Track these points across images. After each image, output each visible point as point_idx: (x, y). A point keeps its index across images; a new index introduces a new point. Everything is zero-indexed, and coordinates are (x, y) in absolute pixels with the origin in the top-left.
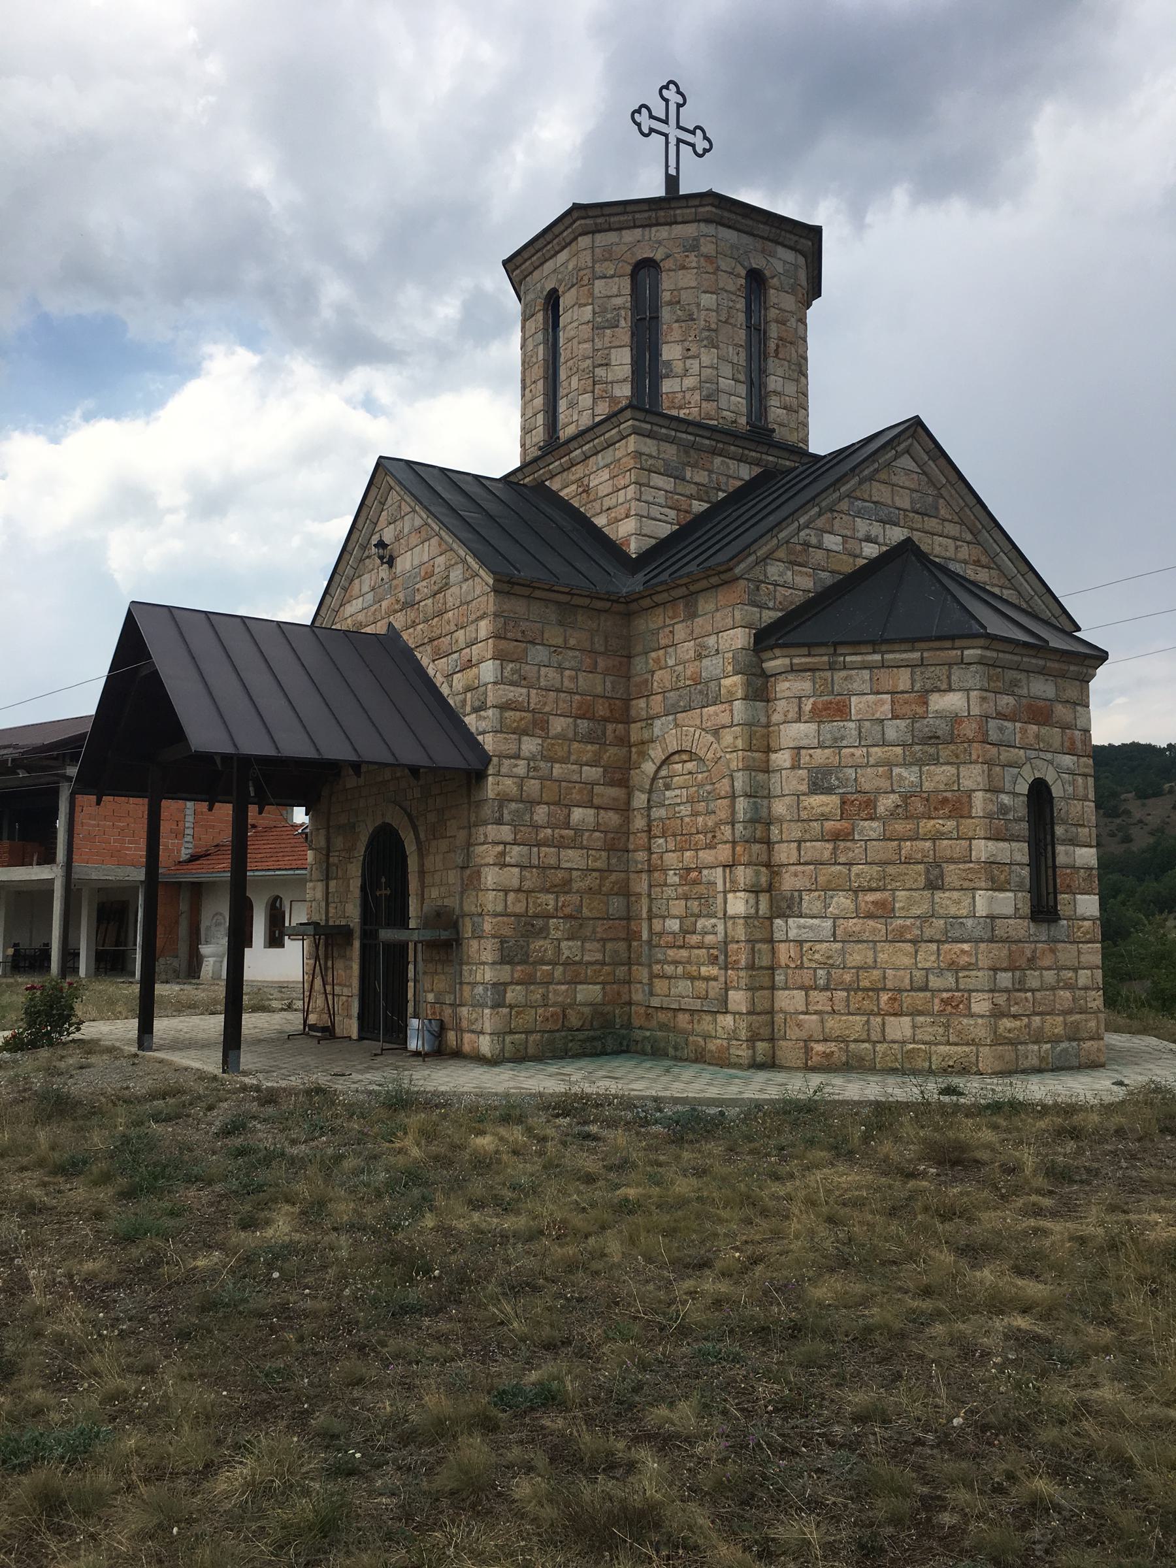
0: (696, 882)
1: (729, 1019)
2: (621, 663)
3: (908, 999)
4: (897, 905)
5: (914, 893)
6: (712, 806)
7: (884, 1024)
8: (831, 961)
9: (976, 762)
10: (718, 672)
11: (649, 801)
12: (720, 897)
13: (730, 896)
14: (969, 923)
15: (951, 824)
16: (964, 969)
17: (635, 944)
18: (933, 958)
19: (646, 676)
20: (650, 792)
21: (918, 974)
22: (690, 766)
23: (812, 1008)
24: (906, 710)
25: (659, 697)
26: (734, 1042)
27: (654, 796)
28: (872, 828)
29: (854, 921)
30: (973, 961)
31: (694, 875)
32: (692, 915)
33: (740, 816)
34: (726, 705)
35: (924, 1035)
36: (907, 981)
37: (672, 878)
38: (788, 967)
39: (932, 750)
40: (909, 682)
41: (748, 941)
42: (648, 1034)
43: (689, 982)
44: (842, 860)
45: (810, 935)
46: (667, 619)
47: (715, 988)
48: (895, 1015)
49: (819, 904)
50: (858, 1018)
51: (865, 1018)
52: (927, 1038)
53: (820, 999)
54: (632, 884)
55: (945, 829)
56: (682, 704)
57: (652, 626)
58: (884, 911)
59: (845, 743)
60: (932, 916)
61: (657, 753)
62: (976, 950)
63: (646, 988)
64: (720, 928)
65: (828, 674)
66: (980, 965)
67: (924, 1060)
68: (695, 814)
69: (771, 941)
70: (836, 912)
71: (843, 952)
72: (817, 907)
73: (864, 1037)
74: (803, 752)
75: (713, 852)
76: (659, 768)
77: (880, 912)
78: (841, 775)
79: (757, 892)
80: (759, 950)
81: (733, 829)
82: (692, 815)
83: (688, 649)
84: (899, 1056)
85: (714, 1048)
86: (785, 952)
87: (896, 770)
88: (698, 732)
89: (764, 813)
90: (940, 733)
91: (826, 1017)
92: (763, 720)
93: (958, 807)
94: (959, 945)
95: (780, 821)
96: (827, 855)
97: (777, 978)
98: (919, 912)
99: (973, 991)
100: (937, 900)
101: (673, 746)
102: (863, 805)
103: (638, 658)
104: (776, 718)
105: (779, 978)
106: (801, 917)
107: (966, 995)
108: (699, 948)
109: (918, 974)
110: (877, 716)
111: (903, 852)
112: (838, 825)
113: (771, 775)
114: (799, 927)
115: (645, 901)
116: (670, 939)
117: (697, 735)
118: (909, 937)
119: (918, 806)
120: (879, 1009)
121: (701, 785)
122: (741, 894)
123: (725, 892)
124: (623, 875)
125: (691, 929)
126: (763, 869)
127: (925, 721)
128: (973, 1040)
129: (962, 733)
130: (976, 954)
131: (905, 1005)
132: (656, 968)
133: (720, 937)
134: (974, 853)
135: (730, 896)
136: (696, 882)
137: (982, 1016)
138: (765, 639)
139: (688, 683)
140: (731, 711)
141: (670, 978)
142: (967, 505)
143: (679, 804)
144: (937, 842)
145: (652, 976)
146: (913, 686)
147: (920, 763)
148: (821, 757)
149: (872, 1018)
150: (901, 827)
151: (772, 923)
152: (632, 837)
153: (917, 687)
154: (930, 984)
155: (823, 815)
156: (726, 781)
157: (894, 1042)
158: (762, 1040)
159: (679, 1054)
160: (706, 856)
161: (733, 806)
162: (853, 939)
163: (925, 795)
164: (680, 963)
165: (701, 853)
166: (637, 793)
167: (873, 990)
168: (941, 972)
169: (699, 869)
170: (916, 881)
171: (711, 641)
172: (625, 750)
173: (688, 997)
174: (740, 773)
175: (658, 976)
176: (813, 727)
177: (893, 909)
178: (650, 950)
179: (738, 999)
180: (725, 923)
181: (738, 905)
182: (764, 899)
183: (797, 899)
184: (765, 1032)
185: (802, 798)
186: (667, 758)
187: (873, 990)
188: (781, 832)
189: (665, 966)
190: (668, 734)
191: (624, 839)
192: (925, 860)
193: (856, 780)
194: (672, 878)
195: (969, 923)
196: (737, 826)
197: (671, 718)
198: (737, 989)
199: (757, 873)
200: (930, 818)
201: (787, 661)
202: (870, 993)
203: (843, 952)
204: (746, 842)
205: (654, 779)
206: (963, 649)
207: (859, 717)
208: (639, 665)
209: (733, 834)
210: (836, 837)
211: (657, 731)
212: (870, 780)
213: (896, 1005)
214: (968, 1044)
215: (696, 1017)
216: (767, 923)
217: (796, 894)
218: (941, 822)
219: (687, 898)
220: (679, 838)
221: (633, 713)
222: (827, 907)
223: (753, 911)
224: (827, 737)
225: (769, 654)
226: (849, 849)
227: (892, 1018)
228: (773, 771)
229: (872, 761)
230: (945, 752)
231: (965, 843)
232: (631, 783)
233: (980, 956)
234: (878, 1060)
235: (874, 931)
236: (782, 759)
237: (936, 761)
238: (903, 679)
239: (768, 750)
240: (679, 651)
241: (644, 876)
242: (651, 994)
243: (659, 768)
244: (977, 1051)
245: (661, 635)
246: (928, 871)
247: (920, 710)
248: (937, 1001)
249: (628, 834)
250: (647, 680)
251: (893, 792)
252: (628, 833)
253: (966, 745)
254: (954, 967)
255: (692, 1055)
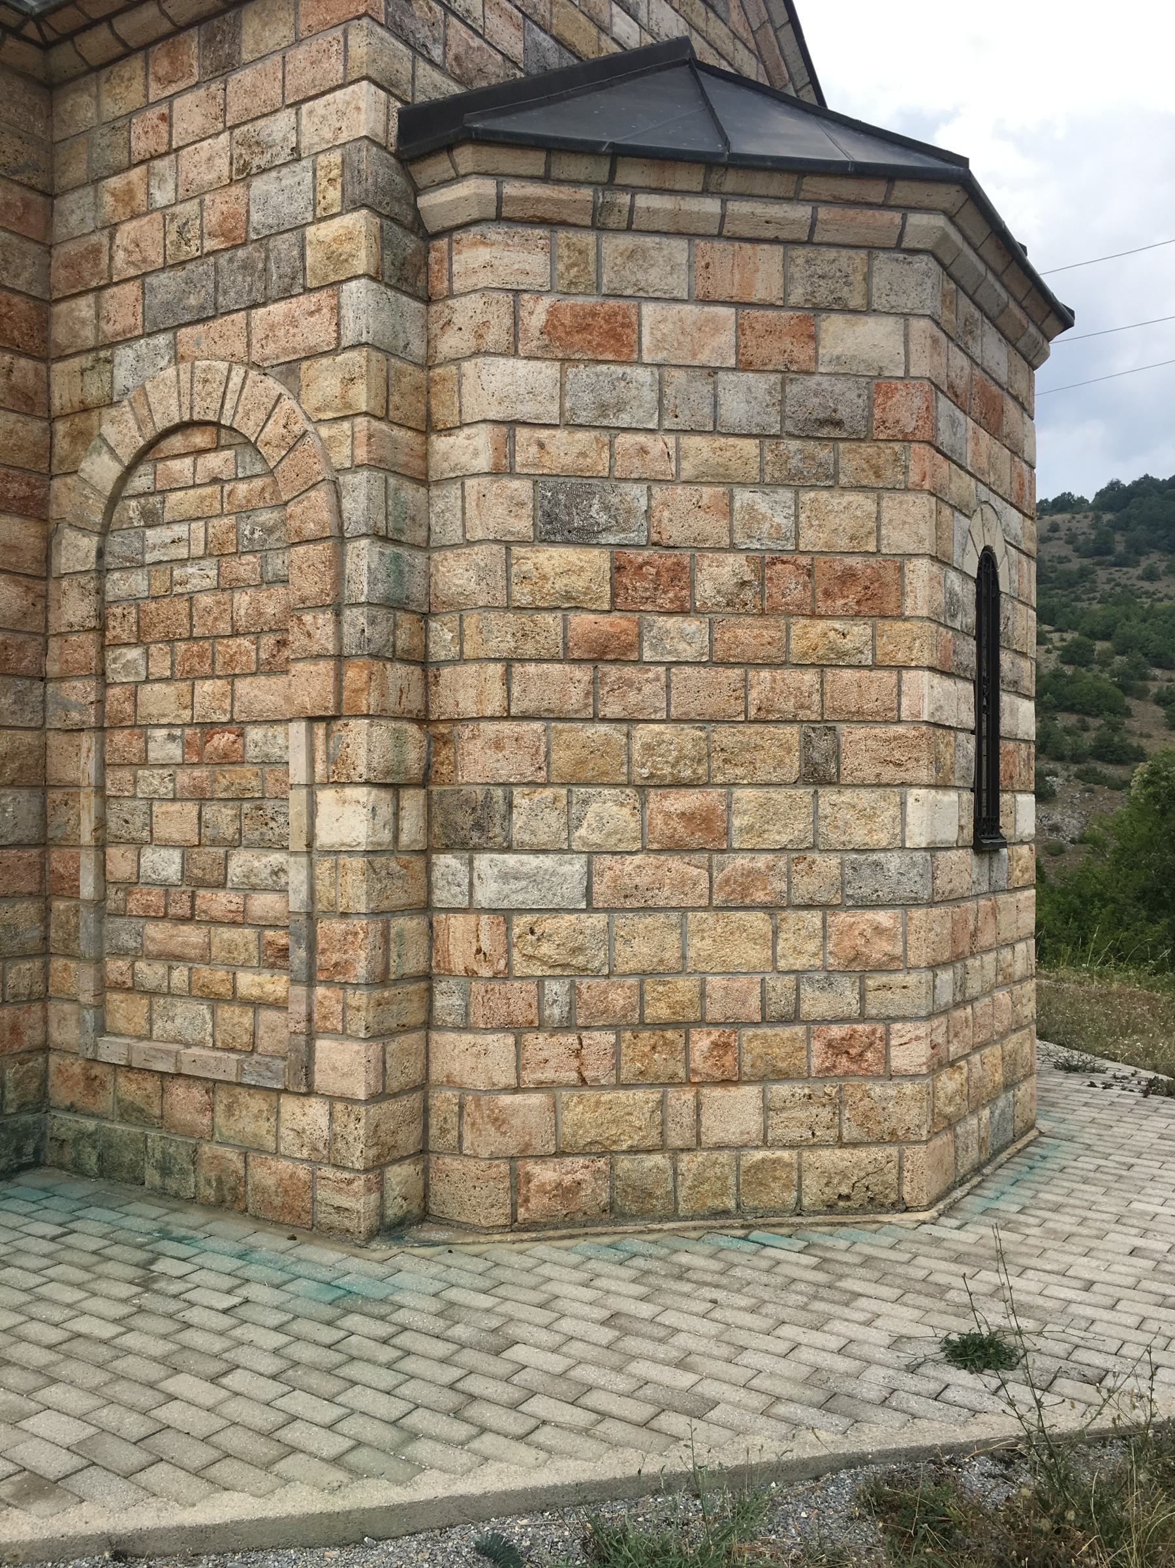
0: (227, 759)
1: (317, 1110)
2: (27, 205)
3: (755, 1044)
4: (737, 822)
5: (774, 794)
6: (277, 563)
7: (698, 1107)
8: (580, 960)
9: (918, 489)
10: (298, 208)
11: (100, 554)
12: (298, 799)
13: (326, 797)
14: (893, 862)
15: (859, 632)
16: (879, 969)
17: (60, 905)
18: (812, 946)
19: (94, 239)
20: (105, 531)
21: (781, 985)
22: (215, 462)
23: (529, 1077)
24: (770, 350)
25: (131, 291)
26: (327, 1172)
27: (116, 543)
28: (684, 635)
29: (638, 859)
30: (898, 951)
31: (222, 740)
32: (214, 842)
33: (360, 588)
34: (323, 295)
35: (788, 1128)
36: (754, 1002)
37: (163, 748)
38: (471, 974)
39: (824, 454)
40: (777, 281)
41: (374, 914)
42: (90, 1125)
43: (204, 1010)
44: (613, 709)
45: (531, 897)
46: (153, 86)
47: (275, 1030)
48: (725, 1082)
49: (553, 819)
50: (640, 1094)
51: (655, 1095)
52: (795, 1134)
53: (550, 1052)
54: (54, 759)
55: (847, 644)
56: (192, 301)
57: (112, 108)
58: (707, 836)
59: (625, 420)
60: (814, 847)
61: (123, 431)
62: (905, 925)
63: (89, 1016)
64: (297, 877)
65: (589, 238)
66: (913, 959)
67: (786, 1187)
68: (227, 586)
69: (426, 908)
70: (596, 838)
71: (609, 937)
72: (549, 825)
73: (653, 1139)
74: (522, 434)
75: (277, 683)
76: (129, 471)
77: (696, 840)
78: (614, 500)
79: (395, 788)
80: (400, 935)
81: (338, 623)
82: (218, 588)
83: (210, 160)
84: (732, 1181)
85: (270, 1182)
86: (461, 939)
87: (743, 497)
88: (238, 373)
89: (416, 588)
90: (843, 413)
91: (565, 1095)
92: (418, 348)
93: (876, 598)
94: (870, 915)
95: (459, 608)
96: (575, 698)
97: (440, 1002)
98: (784, 839)
99: (895, 1019)
100: (825, 809)
101: (168, 412)
102: (665, 578)
103: (72, 197)
104: (450, 343)
105: (447, 1001)
106: (508, 849)
107: (880, 1029)
108: (234, 923)
109: (781, 985)
110: (704, 358)
111: (753, 694)
112: (607, 623)
113: (434, 492)
114: (505, 876)
115: (88, 805)
116: (155, 897)
117: (236, 380)
118: (760, 896)
119: (790, 586)
120: (690, 1071)
121: (245, 511)
122: (360, 793)
123: (311, 787)
124: (28, 738)
125: (214, 876)
126: (412, 729)
127: (812, 382)
128: (893, 1133)
129: (891, 417)
130: (905, 934)
131: (747, 1059)
132: (116, 968)
133: (297, 900)
134: (905, 701)
135: (326, 797)
136: (227, 759)
137: (913, 1077)
138: (426, 133)
139: (210, 244)
140: (337, 309)
141: (152, 993)
142: (771, 20)
143: (183, 562)
144: (829, 674)
145: (104, 986)
146: (787, 294)
147: (796, 482)
148: (566, 449)
149: (672, 1092)
150: (749, 634)
151: (429, 868)
152: (54, 644)
153: (797, 295)
154: (805, 1007)
155: (568, 597)
156: (320, 497)
157: (719, 1147)
158: (401, 1160)
159: (172, 1184)
160: (259, 693)
161: (338, 562)
162: (637, 903)
163: (804, 561)
164: (180, 958)
165: (242, 686)
166: (69, 536)
167: (675, 1025)
168: (828, 977)
169: (238, 727)
170: (781, 763)
171: (279, 126)
172: (37, 427)
173: (201, 1044)
174: (364, 475)
175: (119, 987)
176: (548, 372)
177: (727, 832)
178: (100, 921)
179: (343, 1063)
180: (311, 866)
181: (348, 819)
182: (412, 801)
183: (501, 807)
184: (408, 1139)
185: (517, 551)
186: (152, 445)
187: (675, 1025)
188: (461, 638)
189: (140, 965)
190: (155, 383)
191: (31, 651)
192: (803, 714)
193: (648, 513)
194: (163, 748)
195: (893, 862)
196: (348, 614)
197: (162, 340)
198: (343, 1034)
199: (399, 739)
200: (814, 615)
201: (488, 187)
202: (669, 1034)
203: (609, 937)
204: (374, 656)
205: (114, 499)
206: (907, 209)
207: (659, 357)
208: (76, 213)
209: (339, 635)
210: (601, 654)
211: (123, 376)
212: (681, 516)
213: (729, 1060)
214: (880, 1142)
215: (222, 1098)
216: (418, 864)
217: (499, 793)
218: (837, 625)
219: (201, 798)
220: (181, 647)
221: (59, 334)
222: (572, 825)
223: (386, 836)
224: (584, 405)
225: (438, 167)
226: (629, 683)
227: (718, 1092)
228: (438, 483)
229: (688, 469)
230: (852, 460)
231: (889, 678)
232: (54, 512)
233: (911, 939)
234: (683, 1193)
235: (682, 884)
236: (466, 449)
237: (831, 480)
238: (764, 273)
239: (428, 427)
240: (183, 162)
241: (87, 741)
242: (101, 1029)
243: (129, 471)
244: (901, 1157)
245: (137, 128)
246: (807, 742)
247: (802, 354)
248: (817, 1046)
249: (46, 637)
250: (96, 251)
251: (733, 548)
252: (44, 635)
253: (897, 447)
254: (859, 967)
255: (210, 1193)
